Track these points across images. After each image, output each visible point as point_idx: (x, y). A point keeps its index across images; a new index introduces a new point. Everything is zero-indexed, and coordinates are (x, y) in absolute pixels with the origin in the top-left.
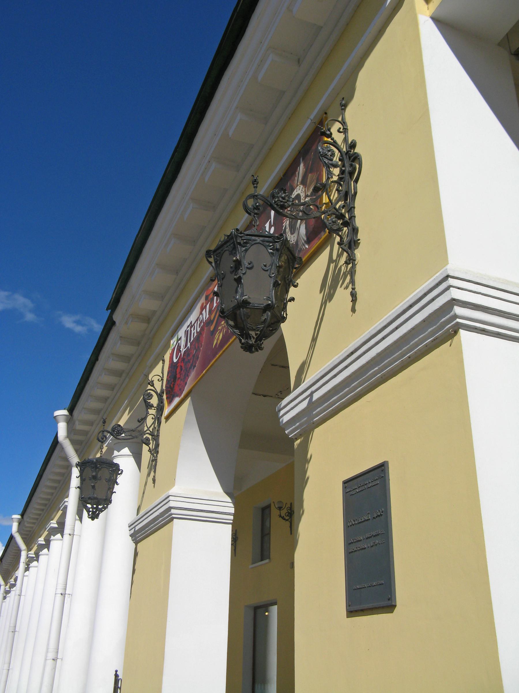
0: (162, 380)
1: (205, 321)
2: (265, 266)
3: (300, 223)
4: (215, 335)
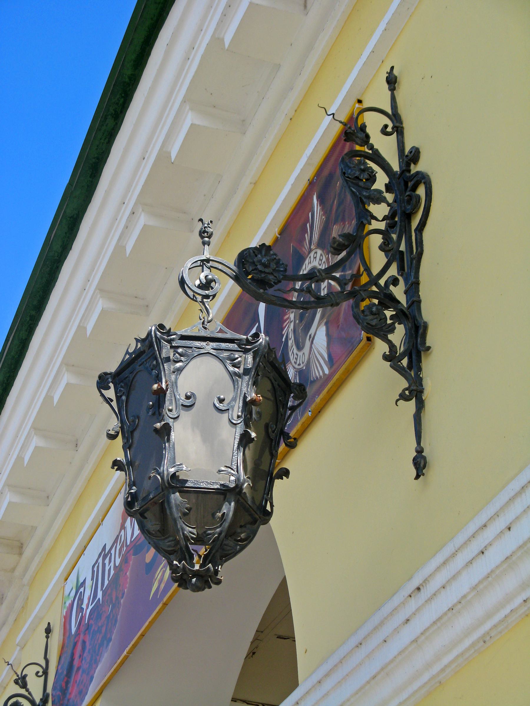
0: (45, 673)
1: (131, 542)
2: (221, 401)
3: (318, 325)
4: (156, 573)
